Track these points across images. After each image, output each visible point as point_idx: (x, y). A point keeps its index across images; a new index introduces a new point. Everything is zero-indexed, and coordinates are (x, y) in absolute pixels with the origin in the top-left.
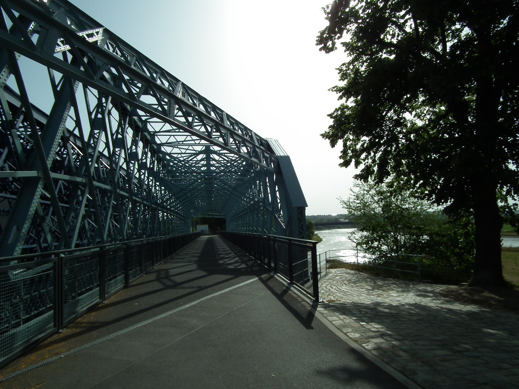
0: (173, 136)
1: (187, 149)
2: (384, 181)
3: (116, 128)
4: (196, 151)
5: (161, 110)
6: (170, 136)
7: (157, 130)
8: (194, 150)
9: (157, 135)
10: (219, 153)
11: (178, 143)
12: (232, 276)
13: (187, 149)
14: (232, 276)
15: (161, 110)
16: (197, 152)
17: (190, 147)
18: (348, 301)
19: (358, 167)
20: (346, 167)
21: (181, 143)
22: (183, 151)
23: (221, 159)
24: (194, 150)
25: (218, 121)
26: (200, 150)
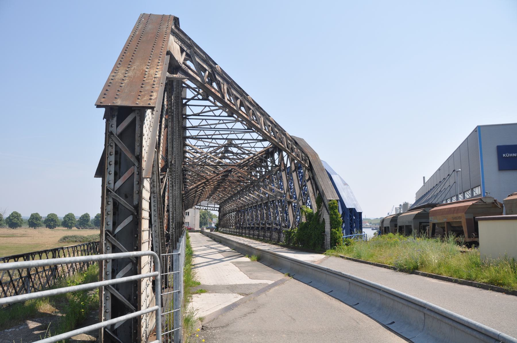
0: (205, 119)
1: (211, 142)
2: (493, 278)
3: (190, 98)
4: (202, 141)
5: (222, 105)
6: (204, 107)
7: (254, 139)
8: (218, 144)
9: (188, 119)
10: (240, 147)
11: (235, 132)
12: (245, 112)
13: (211, 142)
14: (245, 112)
15: (222, 105)
16: (241, 158)
17: (204, 120)
18: (485, 280)
19: (169, 15)
20: (37, 214)
21: (221, 122)
22: (207, 144)
23: (231, 162)
24: (218, 144)
25: (265, 132)
26: (222, 144)
